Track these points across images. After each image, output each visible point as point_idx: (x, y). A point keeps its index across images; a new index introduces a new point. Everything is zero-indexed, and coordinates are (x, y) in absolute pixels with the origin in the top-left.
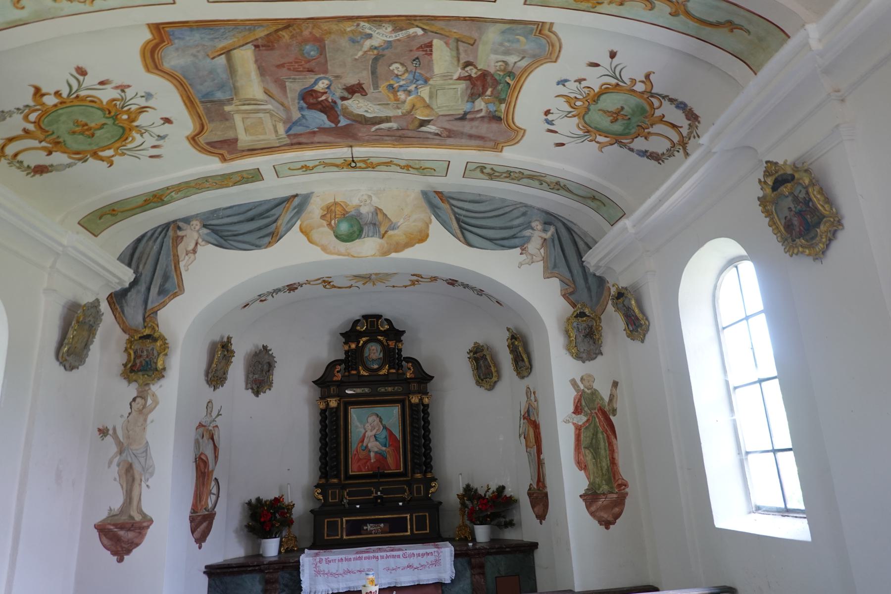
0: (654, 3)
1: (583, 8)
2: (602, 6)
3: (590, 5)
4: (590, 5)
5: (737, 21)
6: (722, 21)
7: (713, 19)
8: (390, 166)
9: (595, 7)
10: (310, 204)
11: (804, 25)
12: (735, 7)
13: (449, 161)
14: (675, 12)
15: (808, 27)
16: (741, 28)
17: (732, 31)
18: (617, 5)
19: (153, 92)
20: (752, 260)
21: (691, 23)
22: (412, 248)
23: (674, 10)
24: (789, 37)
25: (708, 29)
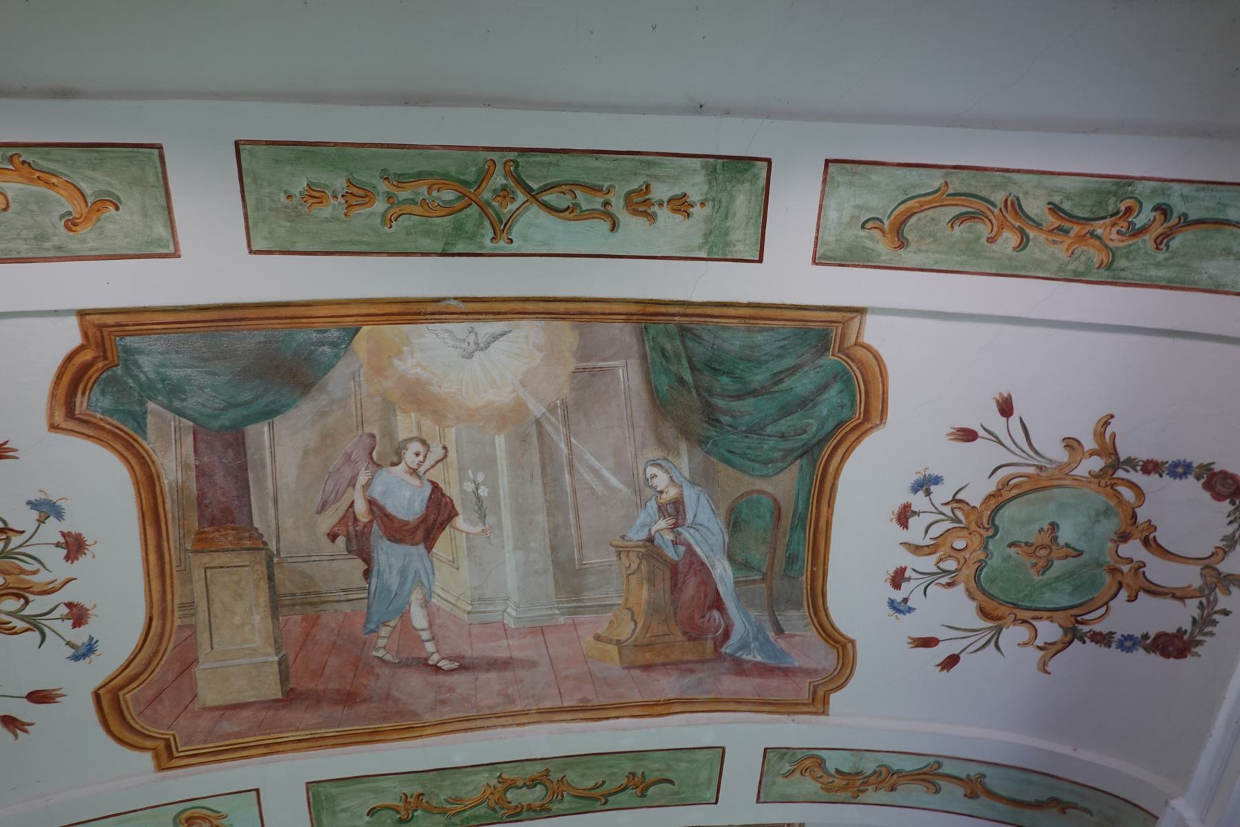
0: (938, 784)
1: (842, 799)
2: (864, 794)
3: (849, 794)
4: (849, 794)
5: (1065, 797)
6: (1044, 799)
7: (1029, 797)
8: (655, 386)
9: (858, 796)
10: (896, 512)
11: (1167, 803)
12: (1053, 779)
13: (257, 790)
14: (972, 792)
15: (1173, 803)
16: (1075, 807)
17: (1063, 811)
18: (886, 791)
19: (1113, 413)
20: (415, 629)
21: (999, 805)
22: (997, 410)
23: (969, 791)
24: (1157, 818)
25: (1028, 812)
